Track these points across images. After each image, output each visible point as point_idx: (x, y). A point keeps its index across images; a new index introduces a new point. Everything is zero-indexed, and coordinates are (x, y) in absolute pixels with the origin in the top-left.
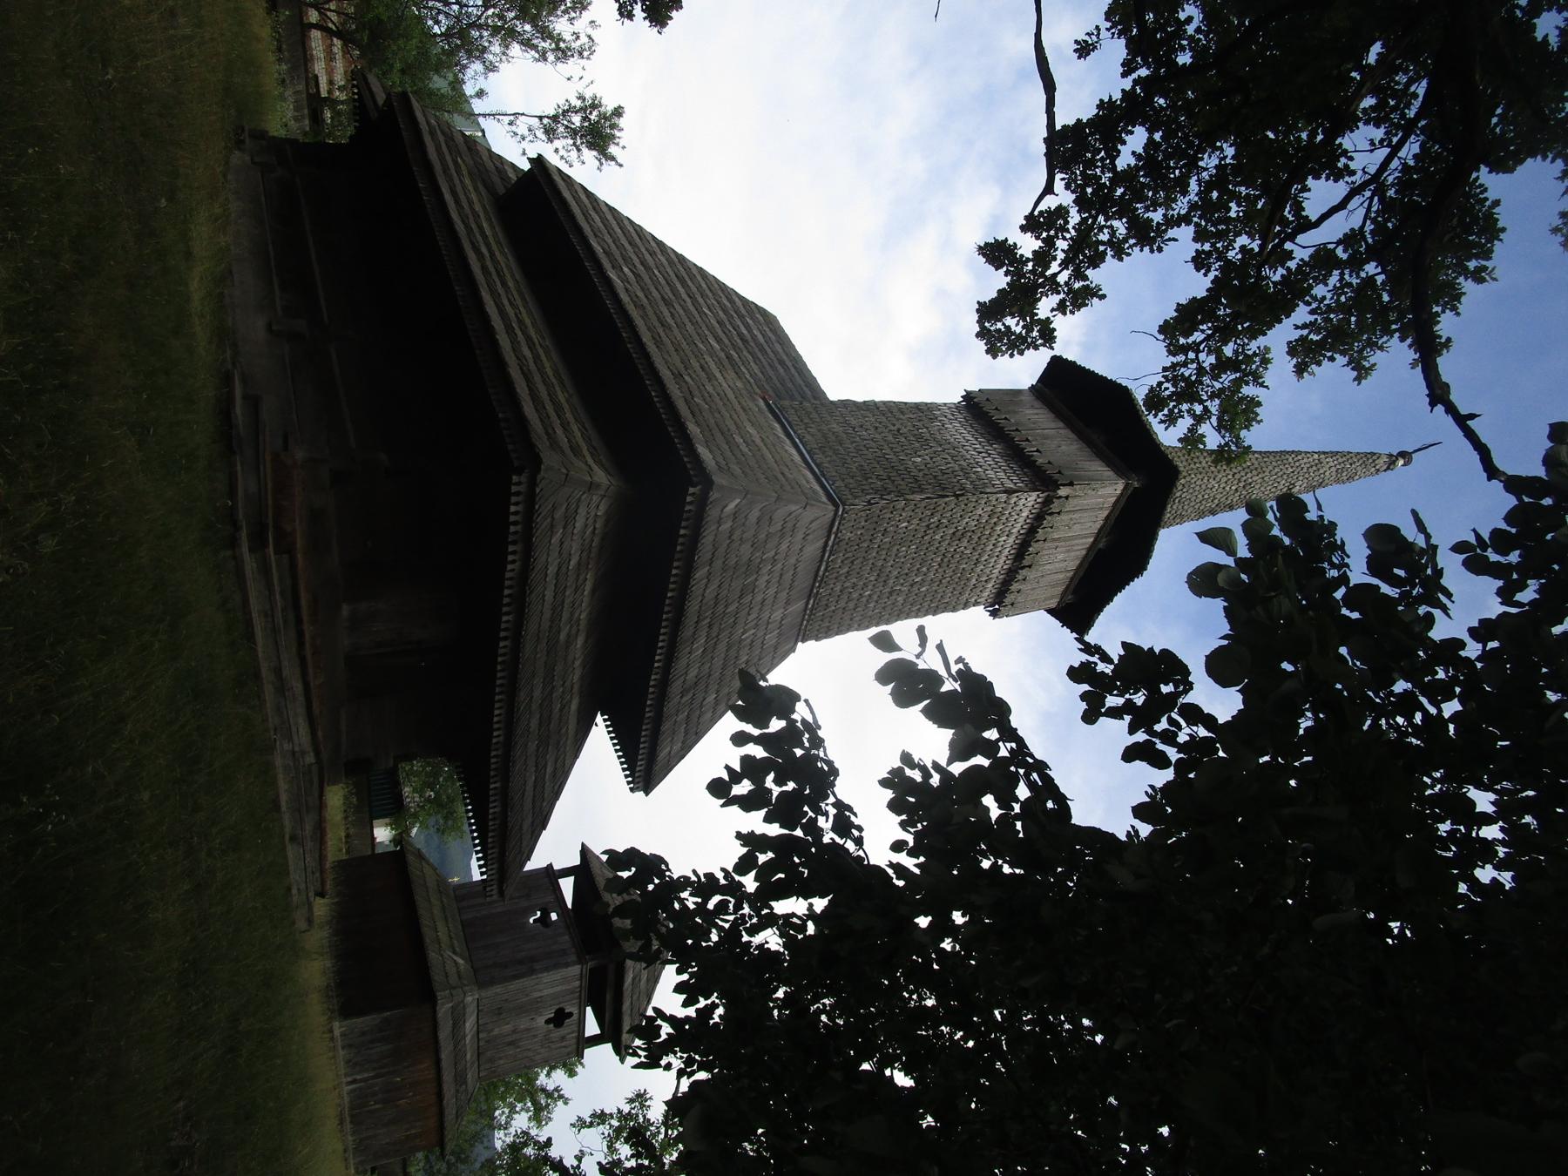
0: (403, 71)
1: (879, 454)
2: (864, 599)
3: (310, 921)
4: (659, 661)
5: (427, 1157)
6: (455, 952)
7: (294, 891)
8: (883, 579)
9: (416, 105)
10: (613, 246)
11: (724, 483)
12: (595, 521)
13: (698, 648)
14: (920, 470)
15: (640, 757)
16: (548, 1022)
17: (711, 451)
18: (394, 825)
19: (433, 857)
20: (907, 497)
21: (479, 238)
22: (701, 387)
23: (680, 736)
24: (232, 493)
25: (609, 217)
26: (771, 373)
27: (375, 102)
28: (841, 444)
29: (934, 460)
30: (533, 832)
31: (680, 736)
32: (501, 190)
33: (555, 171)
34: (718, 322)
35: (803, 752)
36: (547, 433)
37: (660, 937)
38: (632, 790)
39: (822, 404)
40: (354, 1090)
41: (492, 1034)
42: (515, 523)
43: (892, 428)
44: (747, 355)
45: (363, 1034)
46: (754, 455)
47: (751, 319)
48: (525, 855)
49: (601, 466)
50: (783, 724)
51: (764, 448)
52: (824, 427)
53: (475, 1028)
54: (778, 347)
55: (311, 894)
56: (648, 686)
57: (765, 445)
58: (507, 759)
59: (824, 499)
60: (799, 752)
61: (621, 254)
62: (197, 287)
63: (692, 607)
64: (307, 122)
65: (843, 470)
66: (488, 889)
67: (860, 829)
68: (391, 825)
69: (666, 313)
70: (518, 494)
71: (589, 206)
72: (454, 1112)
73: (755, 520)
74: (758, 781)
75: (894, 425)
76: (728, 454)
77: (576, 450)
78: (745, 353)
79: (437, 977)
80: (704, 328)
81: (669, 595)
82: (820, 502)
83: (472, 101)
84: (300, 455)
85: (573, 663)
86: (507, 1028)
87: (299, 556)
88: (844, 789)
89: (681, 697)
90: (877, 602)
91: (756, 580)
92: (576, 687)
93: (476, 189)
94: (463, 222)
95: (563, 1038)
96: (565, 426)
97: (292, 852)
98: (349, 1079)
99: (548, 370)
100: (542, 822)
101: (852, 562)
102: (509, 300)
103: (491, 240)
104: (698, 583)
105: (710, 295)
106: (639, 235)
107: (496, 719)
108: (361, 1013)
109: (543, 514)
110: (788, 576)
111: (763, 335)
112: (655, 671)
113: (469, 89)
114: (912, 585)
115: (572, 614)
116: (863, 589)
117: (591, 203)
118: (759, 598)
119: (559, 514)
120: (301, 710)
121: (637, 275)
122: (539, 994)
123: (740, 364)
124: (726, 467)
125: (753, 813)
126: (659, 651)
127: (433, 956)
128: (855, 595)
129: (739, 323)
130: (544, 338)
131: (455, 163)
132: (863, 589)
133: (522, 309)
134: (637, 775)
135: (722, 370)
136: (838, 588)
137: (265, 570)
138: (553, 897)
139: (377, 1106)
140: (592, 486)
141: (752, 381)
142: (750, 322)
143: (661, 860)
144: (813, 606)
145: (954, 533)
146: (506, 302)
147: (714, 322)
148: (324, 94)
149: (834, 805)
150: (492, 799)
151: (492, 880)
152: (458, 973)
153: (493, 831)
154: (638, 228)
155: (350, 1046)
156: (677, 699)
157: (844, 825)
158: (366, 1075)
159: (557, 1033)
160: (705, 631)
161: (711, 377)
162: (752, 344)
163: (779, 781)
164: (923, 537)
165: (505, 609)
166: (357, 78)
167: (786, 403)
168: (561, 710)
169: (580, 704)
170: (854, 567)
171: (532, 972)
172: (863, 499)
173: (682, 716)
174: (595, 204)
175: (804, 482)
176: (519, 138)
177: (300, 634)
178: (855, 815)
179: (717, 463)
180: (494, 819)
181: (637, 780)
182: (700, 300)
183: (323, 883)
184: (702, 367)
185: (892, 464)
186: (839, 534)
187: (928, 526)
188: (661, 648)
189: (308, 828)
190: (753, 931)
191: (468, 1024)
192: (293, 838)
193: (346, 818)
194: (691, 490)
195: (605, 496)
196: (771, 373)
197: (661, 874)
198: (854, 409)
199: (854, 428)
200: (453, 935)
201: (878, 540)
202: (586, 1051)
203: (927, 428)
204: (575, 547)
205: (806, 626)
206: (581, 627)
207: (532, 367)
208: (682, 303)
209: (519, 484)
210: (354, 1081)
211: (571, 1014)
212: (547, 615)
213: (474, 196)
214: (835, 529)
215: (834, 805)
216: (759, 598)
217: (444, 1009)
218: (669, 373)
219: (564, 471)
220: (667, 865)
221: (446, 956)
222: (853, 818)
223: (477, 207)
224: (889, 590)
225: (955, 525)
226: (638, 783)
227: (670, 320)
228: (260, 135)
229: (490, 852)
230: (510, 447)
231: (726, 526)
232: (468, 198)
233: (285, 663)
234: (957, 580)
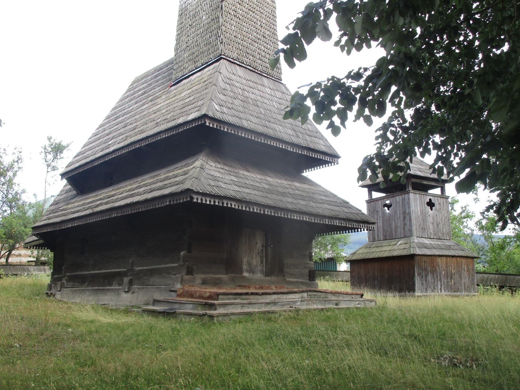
0: (25, 227)
1: (200, 36)
2: (266, 50)
3: (371, 301)
4: (282, 146)
5: (478, 263)
6: (396, 244)
7: (359, 306)
8: (257, 40)
9: (37, 224)
10: (100, 147)
11: (205, 109)
12: (218, 168)
13: (279, 128)
14: (209, 17)
15: (324, 159)
16: (432, 209)
17: (191, 113)
18: (340, 262)
19: (357, 247)
20: (220, 24)
21: (94, 204)
22: (163, 114)
23: (316, 140)
24: (190, 315)
25: (87, 147)
26: (160, 82)
27: (37, 240)
28: (194, 53)
29: (205, 10)
30: (349, 208)
31: (316, 140)
32: (75, 192)
33: (67, 169)
34: (136, 104)
35: (322, 92)
36: (177, 185)
37: (399, 161)
38: (337, 164)
39: (176, 60)
40: (445, 290)
41: (432, 233)
42: (214, 202)
43: (188, 29)
44: (151, 92)
45: (422, 284)
46: (195, 94)
47: (135, 88)
48: (359, 212)
49: (194, 162)
50: (309, 99)
51: (192, 89)
52: (186, 60)
53: (429, 239)
54: (149, 78)
55: (361, 299)
56: (293, 152)
57: (191, 88)
58: (316, 215)
59: (217, 64)
60: (322, 94)
61: (104, 144)
62: (105, 319)
63: (260, 129)
64: (46, 267)
65: (206, 53)
66: (371, 229)
67: (360, 69)
68: (340, 264)
69: (130, 127)
70: (202, 200)
71: (82, 155)
72: (461, 251)
73: (224, 97)
74: (333, 113)
75: (187, 27)
76: (193, 106)
77: (185, 173)
78: (150, 93)
79: (405, 253)
80: (138, 110)
81: (253, 138)
82: (219, 65)
83: (38, 200)
84: (178, 286)
85: (279, 183)
86: (431, 226)
87: (221, 291)
88: (341, 74)
89: (300, 138)
90: (267, 44)
91: (251, 99)
92: (290, 183)
93: (73, 203)
94: (86, 210)
95: (440, 204)
96: (175, 176)
97: (342, 305)
98: (439, 291)
99: (152, 180)
100: (345, 204)
101: (248, 54)
102: (120, 194)
103: (94, 199)
104: (249, 125)
105: (124, 106)
106: (96, 135)
107: (298, 219)
108: (414, 284)
109: (212, 190)
110: (251, 84)
111: (143, 84)
112: (286, 148)
113: (33, 201)
114: (262, 27)
115: (258, 182)
116: (261, 50)
117: (81, 155)
118: (259, 98)
119: (212, 183)
120: (285, 296)
121: (113, 138)
122: (419, 211)
123: (155, 96)
124: (199, 107)
125: (348, 116)
126: (278, 146)
127: (395, 254)
128: (263, 54)
129: (137, 94)
130: (137, 181)
131: (62, 210)
132: (261, 50)
133: (124, 189)
134: (331, 161)
135: (156, 104)
136: (259, 61)
137: (224, 305)
138: (379, 201)
139: (453, 281)
140: (202, 168)
141: (163, 91)
142: (137, 89)
143: (366, 158)
144: (266, 74)
145: (240, 4)
146: (121, 196)
147: (136, 106)
148: (35, 259)
149: (348, 79)
150: (332, 224)
151: (367, 227)
152: (404, 244)
153: (346, 224)
154: (93, 135)
155: (426, 289)
156: (300, 140)
157: (357, 76)
158: (439, 285)
159: (437, 206)
160: (271, 124)
161: (159, 110)
162: (146, 89)
163: (335, 104)
164: (240, 19)
165: (251, 210)
166: (28, 246)
167: (174, 77)
168: (298, 190)
169: (297, 182)
170: (250, 53)
171: (409, 213)
172: (219, 46)
173: (308, 138)
174: (82, 153)
175: (209, 72)
176: (55, 182)
177: (252, 294)
178: (353, 70)
179: (197, 111)
180: (341, 223)
181: (334, 161)
182: (126, 111)
183: (357, 294)
184: (154, 113)
185: (205, 30)
186: (235, 58)
187: (235, 16)
188: (276, 144)
189: (334, 298)
190: (405, 121)
191: (426, 242)
192: (337, 304)
193: (334, 281)
194: (207, 124)
195: (207, 163)
196: (160, 82)
197: (372, 159)
198: (179, 45)
199: (187, 46)
200: (389, 244)
201: (239, 41)
202: (446, 195)
203: (190, 12)
204: (228, 178)
205: (275, 78)
206: (264, 178)
207: (149, 188)
208: (126, 119)
209: (197, 199)
210: (441, 289)
211: (430, 200)
212: (256, 192)
213: (76, 204)
214: (232, 60)
215: (348, 79)
216: (259, 98)
217: (418, 252)
218: (156, 128)
219: (194, 179)
220: (369, 156)
221: (397, 248)
222: (355, 71)
223: (81, 203)
224: (262, 38)
225: (236, 3)
226: (335, 160)
227: (133, 125)
228: (50, 287)
229: (355, 227)
230: (181, 201)
231: (225, 110)
232: (76, 207)
233: (264, 301)
234: (261, 5)
